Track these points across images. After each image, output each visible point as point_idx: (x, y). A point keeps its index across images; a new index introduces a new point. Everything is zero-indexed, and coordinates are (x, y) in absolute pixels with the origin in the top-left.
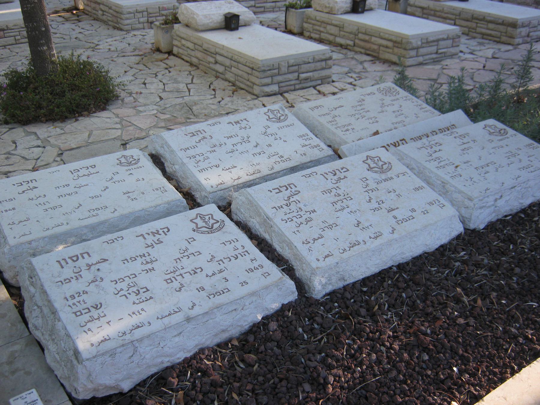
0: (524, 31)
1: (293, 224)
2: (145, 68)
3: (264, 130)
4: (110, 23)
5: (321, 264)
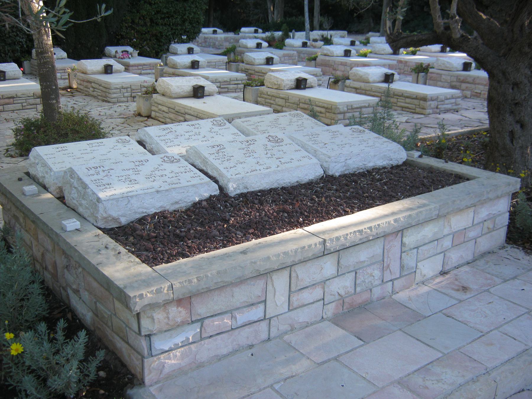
0: (433, 104)
1: (220, 161)
2: (128, 126)
3: (210, 130)
4: (99, 97)
5: (234, 177)
